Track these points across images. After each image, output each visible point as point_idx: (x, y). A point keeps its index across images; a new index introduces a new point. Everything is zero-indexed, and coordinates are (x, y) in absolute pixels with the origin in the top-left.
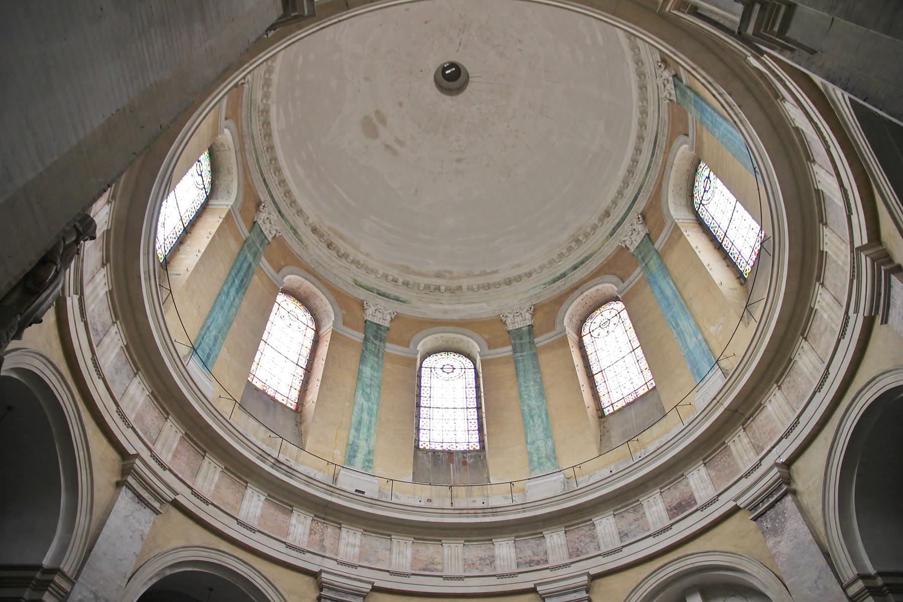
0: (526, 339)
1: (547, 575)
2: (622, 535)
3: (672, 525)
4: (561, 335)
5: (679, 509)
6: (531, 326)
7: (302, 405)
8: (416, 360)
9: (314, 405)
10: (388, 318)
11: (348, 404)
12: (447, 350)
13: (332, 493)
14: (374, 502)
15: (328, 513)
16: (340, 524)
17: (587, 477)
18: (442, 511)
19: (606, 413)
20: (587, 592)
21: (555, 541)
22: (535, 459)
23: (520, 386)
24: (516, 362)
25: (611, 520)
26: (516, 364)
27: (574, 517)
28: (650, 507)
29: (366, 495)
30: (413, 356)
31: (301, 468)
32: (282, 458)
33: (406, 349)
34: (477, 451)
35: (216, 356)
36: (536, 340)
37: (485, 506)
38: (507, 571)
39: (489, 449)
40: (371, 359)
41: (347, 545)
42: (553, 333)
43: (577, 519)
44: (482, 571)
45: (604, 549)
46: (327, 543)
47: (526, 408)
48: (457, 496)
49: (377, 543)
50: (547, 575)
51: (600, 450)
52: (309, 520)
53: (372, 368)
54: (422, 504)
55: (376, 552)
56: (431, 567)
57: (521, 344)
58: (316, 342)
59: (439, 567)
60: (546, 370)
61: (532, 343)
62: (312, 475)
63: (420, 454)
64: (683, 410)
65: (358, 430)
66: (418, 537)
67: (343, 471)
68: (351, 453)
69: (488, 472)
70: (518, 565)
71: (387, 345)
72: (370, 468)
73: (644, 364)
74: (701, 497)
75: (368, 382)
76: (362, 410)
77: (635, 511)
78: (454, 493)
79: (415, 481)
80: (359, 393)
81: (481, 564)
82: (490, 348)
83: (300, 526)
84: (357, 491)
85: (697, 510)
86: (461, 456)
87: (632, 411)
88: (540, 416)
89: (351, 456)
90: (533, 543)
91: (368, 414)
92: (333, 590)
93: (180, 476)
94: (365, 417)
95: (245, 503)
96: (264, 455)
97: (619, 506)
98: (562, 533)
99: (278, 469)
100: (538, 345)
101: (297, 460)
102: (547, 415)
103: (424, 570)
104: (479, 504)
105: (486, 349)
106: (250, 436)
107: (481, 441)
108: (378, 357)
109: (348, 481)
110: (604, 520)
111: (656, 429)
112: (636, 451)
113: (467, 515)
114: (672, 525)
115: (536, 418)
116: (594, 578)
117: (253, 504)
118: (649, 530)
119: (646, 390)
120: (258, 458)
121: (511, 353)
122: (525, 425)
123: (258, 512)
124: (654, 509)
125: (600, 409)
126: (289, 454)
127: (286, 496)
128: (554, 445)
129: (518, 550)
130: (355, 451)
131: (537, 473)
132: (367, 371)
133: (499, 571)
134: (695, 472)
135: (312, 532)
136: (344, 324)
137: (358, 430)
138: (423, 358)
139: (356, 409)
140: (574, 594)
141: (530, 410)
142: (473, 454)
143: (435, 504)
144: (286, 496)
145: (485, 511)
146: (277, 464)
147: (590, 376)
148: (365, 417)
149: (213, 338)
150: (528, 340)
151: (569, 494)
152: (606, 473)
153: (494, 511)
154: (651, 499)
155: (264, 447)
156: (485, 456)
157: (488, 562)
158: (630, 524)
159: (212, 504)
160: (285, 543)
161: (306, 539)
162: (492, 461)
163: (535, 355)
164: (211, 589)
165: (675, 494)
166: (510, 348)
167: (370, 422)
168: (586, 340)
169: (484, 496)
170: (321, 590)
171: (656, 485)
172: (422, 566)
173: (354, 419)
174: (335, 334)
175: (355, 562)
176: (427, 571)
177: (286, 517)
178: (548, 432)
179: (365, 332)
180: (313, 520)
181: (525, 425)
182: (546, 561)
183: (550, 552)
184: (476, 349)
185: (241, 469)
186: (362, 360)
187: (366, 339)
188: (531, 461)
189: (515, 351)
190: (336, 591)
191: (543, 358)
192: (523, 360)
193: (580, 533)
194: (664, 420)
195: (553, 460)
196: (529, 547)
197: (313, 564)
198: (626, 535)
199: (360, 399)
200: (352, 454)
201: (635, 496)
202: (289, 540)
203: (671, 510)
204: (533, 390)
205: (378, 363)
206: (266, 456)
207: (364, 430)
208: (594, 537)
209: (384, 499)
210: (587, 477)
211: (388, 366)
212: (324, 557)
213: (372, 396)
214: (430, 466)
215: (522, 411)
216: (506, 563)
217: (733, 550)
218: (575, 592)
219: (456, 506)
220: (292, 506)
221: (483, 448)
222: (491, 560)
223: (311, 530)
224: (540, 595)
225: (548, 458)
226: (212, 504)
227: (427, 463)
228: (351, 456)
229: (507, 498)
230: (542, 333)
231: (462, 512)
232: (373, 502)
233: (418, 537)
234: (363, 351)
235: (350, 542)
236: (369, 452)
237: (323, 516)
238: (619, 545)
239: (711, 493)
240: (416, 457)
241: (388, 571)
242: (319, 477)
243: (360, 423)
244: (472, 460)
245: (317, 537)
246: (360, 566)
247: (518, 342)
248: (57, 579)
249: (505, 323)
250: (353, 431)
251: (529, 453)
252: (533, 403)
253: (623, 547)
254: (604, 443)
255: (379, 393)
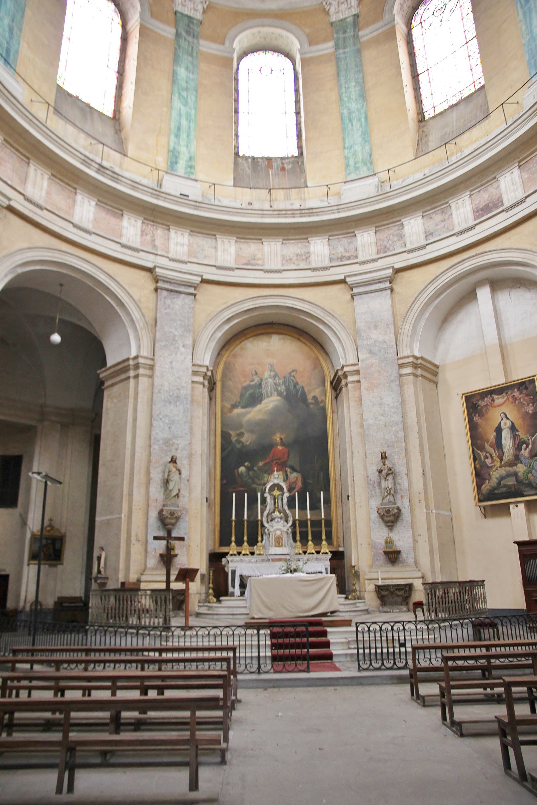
0: (350, 32)
1: (357, 268)
2: (428, 234)
3: (476, 225)
4: (390, 26)
5: (483, 212)
6: (356, 16)
7: (119, 112)
8: (232, 60)
9: (131, 111)
10: (200, 8)
11: (165, 109)
12: (265, 49)
13: (158, 197)
14: (198, 204)
15: (156, 215)
16: (169, 226)
17: (400, 181)
18: (262, 212)
19: (427, 117)
20: (390, 283)
21: (366, 240)
22: (352, 163)
23: (340, 87)
24: (338, 60)
25: (420, 220)
26: (337, 63)
27: (383, 218)
28: (457, 208)
29: (190, 198)
30: (228, 55)
31: (126, 174)
32: (105, 164)
33: (221, 47)
34: (296, 157)
35: (17, 52)
36: (361, 33)
37: (302, 207)
38: (320, 265)
39: (307, 153)
40: (185, 59)
41: (177, 244)
42: (380, 24)
43: (387, 220)
44: (298, 265)
45: (409, 247)
46: (158, 243)
47: (345, 111)
48: (276, 200)
49: (203, 243)
50: (357, 268)
51: (416, 154)
52: (139, 223)
53: (187, 69)
54: (244, 206)
55: (203, 250)
56: (253, 262)
57: (344, 39)
58: (125, 39)
59: (260, 262)
60: (369, 69)
61: (356, 37)
62: (138, 180)
63: (240, 161)
64: (509, 109)
65: (177, 136)
66: (240, 236)
67: (167, 177)
68: (173, 158)
69: (306, 177)
70: (331, 260)
71: (202, 42)
72: (192, 173)
73: (476, 58)
74: (508, 200)
75: (184, 84)
76: (180, 115)
77: (443, 212)
78: (273, 197)
79: (235, 186)
80: (176, 97)
81: (297, 259)
82: (311, 44)
83: (131, 228)
84: (181, 194)
85: (503, 211)
86: (279, 162)
87: (454, 115)
88: (359, 120)
89: (173, 162)
90: (345, 241)
91: (187, 119)
92: (167, 282)
93: (9, 182)
94: (184, 123)
95: (77, 208)
96: (87, 161)
97: (429, 208)
98: (372, 232)
99: (104, 174)
100: (362, 40)
101: (121, 167)
102: (366, 118)
103: (247, 264)
104: (296, 206)
105: (306, 45)
106: (71, 141)
107: (300, 147)
108: (192, 56)
109: (173, 185)
110: (412, 221)
111: (476, 132)
112: (452, 154)
113: (286, 216)
114: (476, 225)
115: (355, 122)
116: (398, 271)
117: (85, 209)
118: (453, 229)
119: (473, 90)
120: (82, 163)
121: (332, 50)
122: (344, 130)
123: (91, 216)
124: (461, 210)
125: (421, 113)
126: (112, 159)
127: (115, 201)
128: (371, 149)
129: (331, 247)
130: (176, 157)
131: (353, 176)
132: (182, 72)
133: (313, 265)
134: (508, 175)
135: (143, 233)
136: (152, 15)
137: (177, 136)
138: (240, 58)
139: (174, 114)
140: (379, 285)
141: (350, 114)
142: (291, 160)
143: (256, 206)
144: (115, 201)
145: (301, 212)
146: (101, 169)
147: (415, 76)
148: (184, 123)
149: (7, 29)
150: (352, 34)
151: (383, 196)
152: (420, 176)
153: (311, 211)
154: (460, 202)
155: (87, 154)
156: (303, 162)
157: (304, 257)
158: (437, 225)
159: (46, 209)
160: (120, 243)
161: (138, 239)
162: (310, 166)
163: (359, 52)
164: (61, 285)
165: (484, 197)
166: (331, 44)
167: (189, 127)
168: (416, 32)
169: (301, 199)
170: (157, 282)
171: (466, 188)
172: (244, 261)
173: (173, 125)
174: (143, 28)
175: (185, 258)
176: (249, 265)
177: (118, 220)
178: (366, 136)
179: (176, 27)
180: (143, 223)
181: (344, 130)
182: (356, 257)
183: (360, 249)
184: (295, 45)
185: (68, 176)
186: (176, 60)
187: (178, 35)
188: (347, 166)
189: (337, 47)
190: (170, 283)
191: (368, 55)
192: (346, 58)
193: (388, 233)
194: (487, 121)
195: (369, 165)
196: (341, 245)
197: (148, 261)
198: (432, 234)
199: (177, 104)
200: (174, 160)
201: (445, 198)
202: (124, 241)
203: (478, 212)
204: (354, 91)
205: (192, 64)
206: (90, 162)
207: (184, 136)
208: (401, 236)
209: (206, 202)
210: (400, 181)
211: (204, 66)
212: (156, 255)
213: (189, 101)
214: (249, 171)
215: (342, 115)
216: (320, 259)
217: (528, 247)
218: (380, 282)
219: (275, 207)
220: (122, 211)
221: (301, 154)
222: (307, 256)
223: (142, 231)
224: (349, 285)
225: (364, 163)
226: (46, 209)
227: (247, 169)
228: (173, 162)
229: (322, 201)
230: (367, 25)
231: (280, 212)
232: (197, 205)
233: (240, 236)
234: (176, 49)
235: (180, 241)
236: (191, 158)
237: (152, 219)
238: (423, 242)
239: (520, 195)
240: (236, 164)
241: (215, 266)
242: (145, 182)
243: (179, 129)
244: (290, 166)
245: (149, 238)
246: (189, 262)
247: (341, 36)
248: (158, 277)
249: (327, 13)
250: (172, 137)
251: (346, 158)
252: (353, 106)
253: (427, 245)
254: (421, 148)
255: (196, 97)
